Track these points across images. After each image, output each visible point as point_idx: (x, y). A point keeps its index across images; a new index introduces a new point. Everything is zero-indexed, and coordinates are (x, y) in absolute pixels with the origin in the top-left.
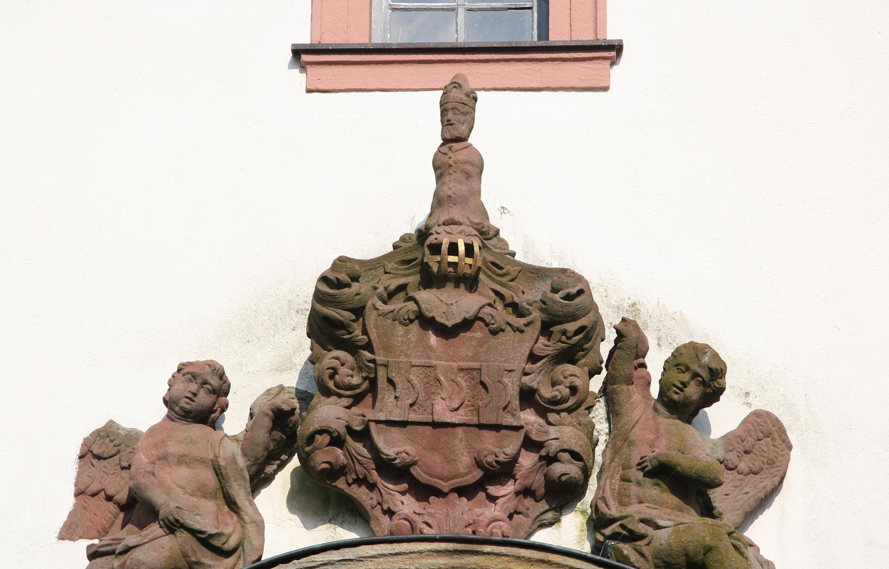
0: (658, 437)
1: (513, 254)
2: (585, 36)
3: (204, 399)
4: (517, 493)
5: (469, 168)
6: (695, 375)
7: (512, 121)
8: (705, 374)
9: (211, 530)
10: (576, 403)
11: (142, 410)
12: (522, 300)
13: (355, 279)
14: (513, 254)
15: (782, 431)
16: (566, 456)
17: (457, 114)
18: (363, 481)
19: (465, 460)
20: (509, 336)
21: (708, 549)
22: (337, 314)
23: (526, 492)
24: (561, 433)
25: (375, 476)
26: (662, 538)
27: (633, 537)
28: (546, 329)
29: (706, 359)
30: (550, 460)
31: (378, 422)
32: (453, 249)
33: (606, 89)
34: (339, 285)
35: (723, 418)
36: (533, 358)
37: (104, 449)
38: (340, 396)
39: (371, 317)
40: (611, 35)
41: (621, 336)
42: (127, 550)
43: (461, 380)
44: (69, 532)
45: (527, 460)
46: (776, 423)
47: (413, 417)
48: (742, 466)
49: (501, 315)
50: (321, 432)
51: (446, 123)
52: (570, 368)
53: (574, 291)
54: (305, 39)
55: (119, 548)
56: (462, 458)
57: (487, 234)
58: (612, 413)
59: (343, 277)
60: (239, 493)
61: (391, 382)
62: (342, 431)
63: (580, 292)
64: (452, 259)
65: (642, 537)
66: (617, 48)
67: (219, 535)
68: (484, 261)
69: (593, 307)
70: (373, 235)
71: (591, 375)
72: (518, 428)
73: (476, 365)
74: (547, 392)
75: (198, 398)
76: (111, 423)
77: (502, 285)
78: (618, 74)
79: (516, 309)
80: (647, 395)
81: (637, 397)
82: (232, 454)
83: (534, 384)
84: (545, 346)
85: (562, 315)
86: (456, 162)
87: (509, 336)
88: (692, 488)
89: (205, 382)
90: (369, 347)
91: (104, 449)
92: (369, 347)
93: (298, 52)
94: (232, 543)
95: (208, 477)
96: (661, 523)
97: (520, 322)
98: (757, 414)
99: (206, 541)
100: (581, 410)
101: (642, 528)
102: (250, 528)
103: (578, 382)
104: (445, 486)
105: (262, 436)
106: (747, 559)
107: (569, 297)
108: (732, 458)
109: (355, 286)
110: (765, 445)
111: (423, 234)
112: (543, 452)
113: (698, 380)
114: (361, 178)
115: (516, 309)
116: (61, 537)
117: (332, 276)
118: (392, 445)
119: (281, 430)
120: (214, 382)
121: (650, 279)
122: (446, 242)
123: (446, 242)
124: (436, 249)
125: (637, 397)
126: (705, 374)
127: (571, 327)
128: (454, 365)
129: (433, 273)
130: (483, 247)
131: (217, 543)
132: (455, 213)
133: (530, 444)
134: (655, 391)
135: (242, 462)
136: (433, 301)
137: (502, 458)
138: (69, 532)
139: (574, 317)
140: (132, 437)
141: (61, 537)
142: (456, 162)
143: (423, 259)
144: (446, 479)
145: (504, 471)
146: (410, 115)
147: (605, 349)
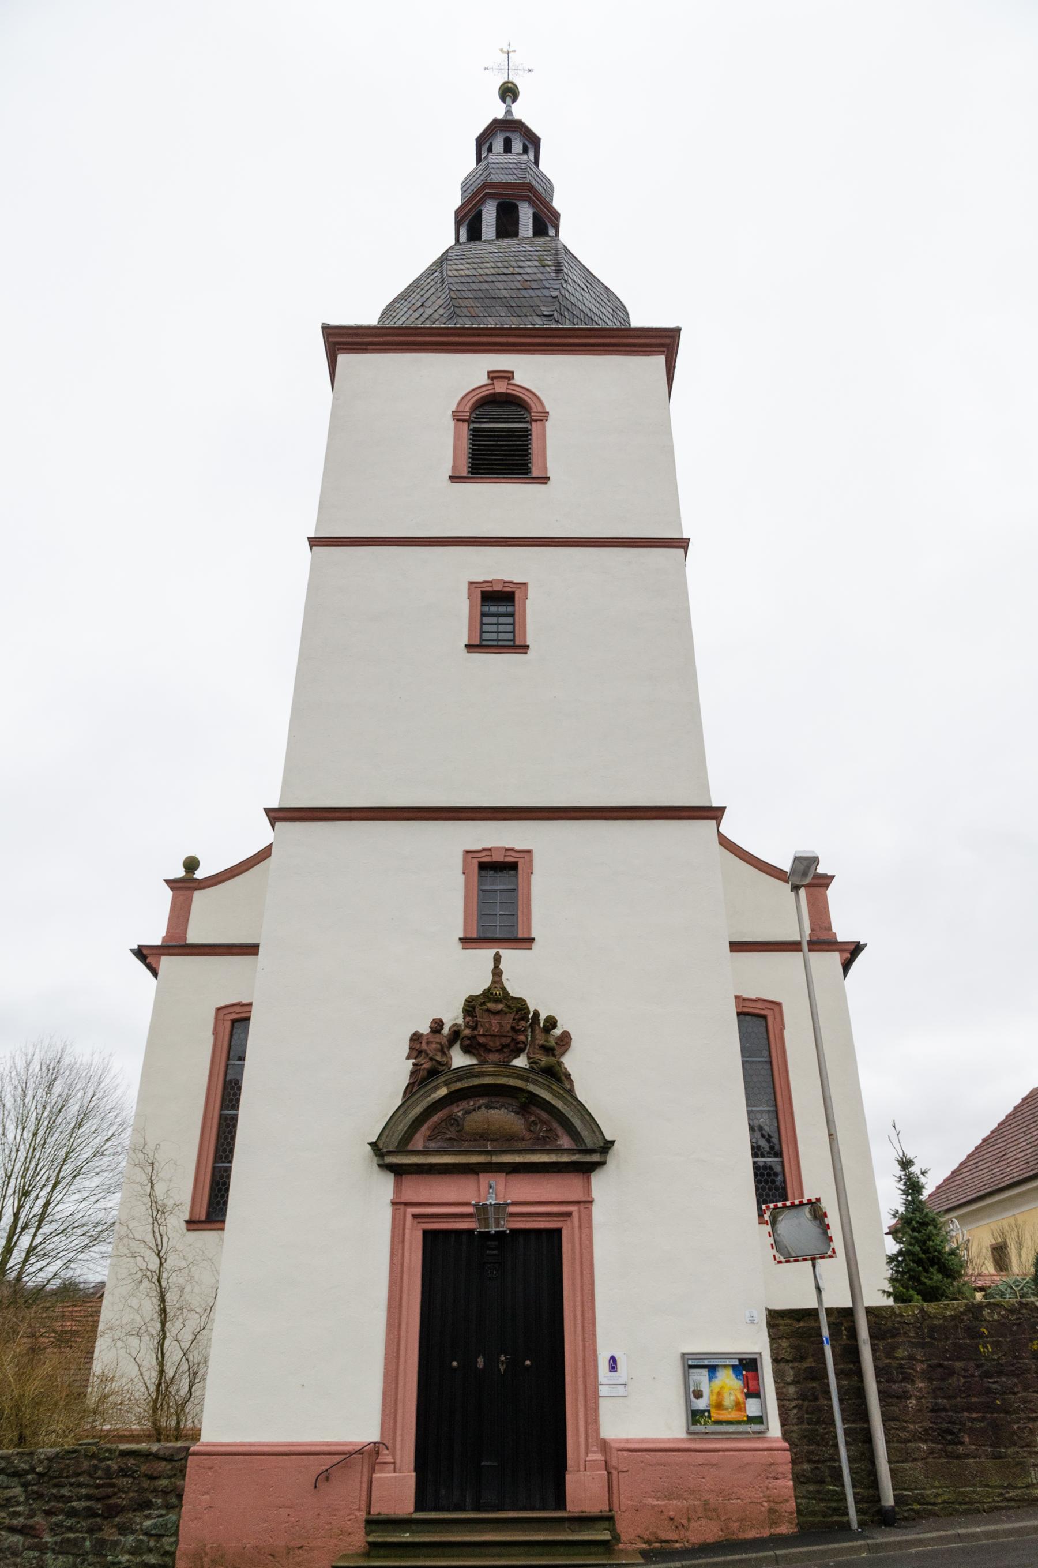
0: (540, 1039)
2: (526, 936)
7: (510, 957)
11: (425, 1029)
19: (498, 1044)
22: (471, 1006)
23: (512, 1051)
24: (522, 1038)
28: (517, 1013)
35: (557, 1032)
37: (416, 1038)
39: (477, 1010)
44: (408, 1058)
49: (506, 1010)
57: (504, 989)
60: (446, 1050)
75: (437, 1026)
78: (534, 945)
82: (445, 1041)
85: (519, 1007)
86: (497, 973)
88: (548, 1050)
95: (439, 1046)
99: (439, 1063)
110: (565, 1040)
113: (552, 1023)
114: (473, 971)
116: (265, 809)
118: (481, 1040)
119: (456, 1035)
121: (541, 1002)
129: (484, 1357)
136: (491, 1005)
138: (408, 1058)
140: (422, 1035)
141: (265, 809)
142: (497, 973)
143: (487, 994)
145: (508, 1046)
146: (485, 956)
147: (530, 1016)
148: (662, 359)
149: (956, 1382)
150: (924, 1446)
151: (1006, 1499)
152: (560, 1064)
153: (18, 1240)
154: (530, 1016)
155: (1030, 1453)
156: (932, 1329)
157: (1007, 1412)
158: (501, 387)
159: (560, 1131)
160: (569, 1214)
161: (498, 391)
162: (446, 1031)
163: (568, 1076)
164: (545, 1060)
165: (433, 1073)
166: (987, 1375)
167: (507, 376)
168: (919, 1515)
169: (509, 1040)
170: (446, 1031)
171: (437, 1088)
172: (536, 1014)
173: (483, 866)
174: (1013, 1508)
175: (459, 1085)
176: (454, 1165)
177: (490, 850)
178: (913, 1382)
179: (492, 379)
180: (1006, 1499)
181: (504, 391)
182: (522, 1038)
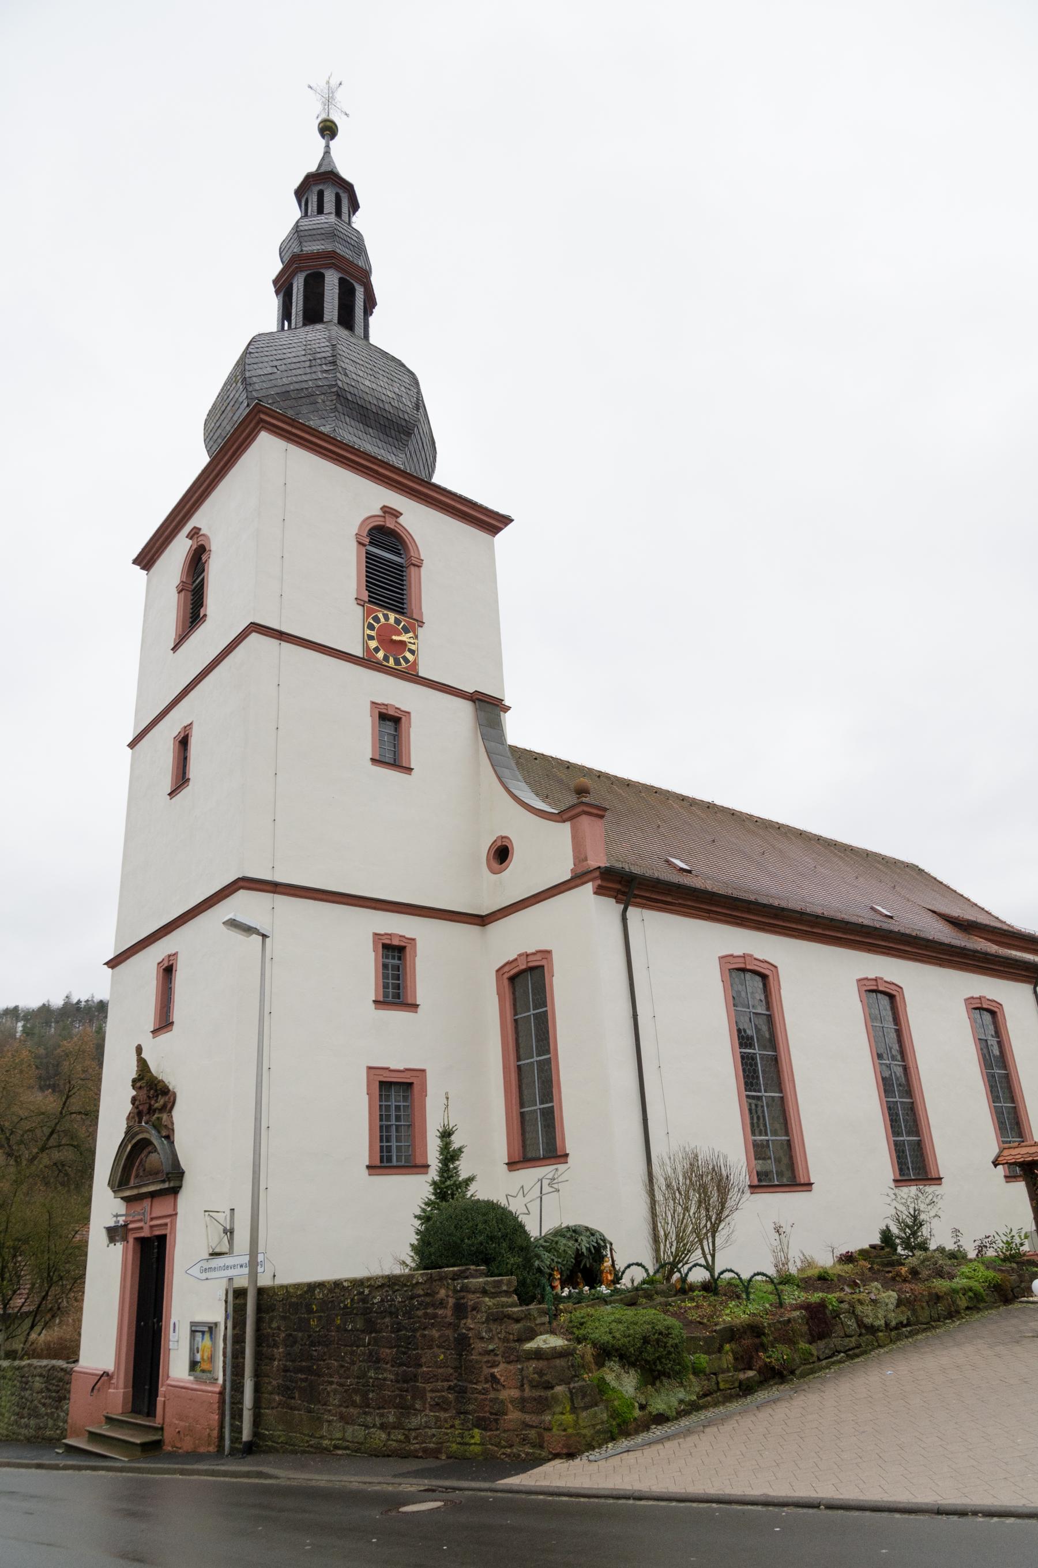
148: (622, 906)
149: (297, 1348)
150: (277, 1398)
151: (312, 1446)
153: (835, 854)
155: (325, 1410)
156: (292, 1304)
157: (319, 1376)
158: (390, 524)
160: (166, 1224)
161: (388, 525)
166: (313, 1344)
167: (396, 514)
168: (270, 1450)
173: (386, 947)
174: (312, 1453)
175: (134, 1141)
176: (161, 1190)
177: (390, 935)
178: (278, 1348)
179: (385, 512)
180: (312, 1446)
181: (392, 527)
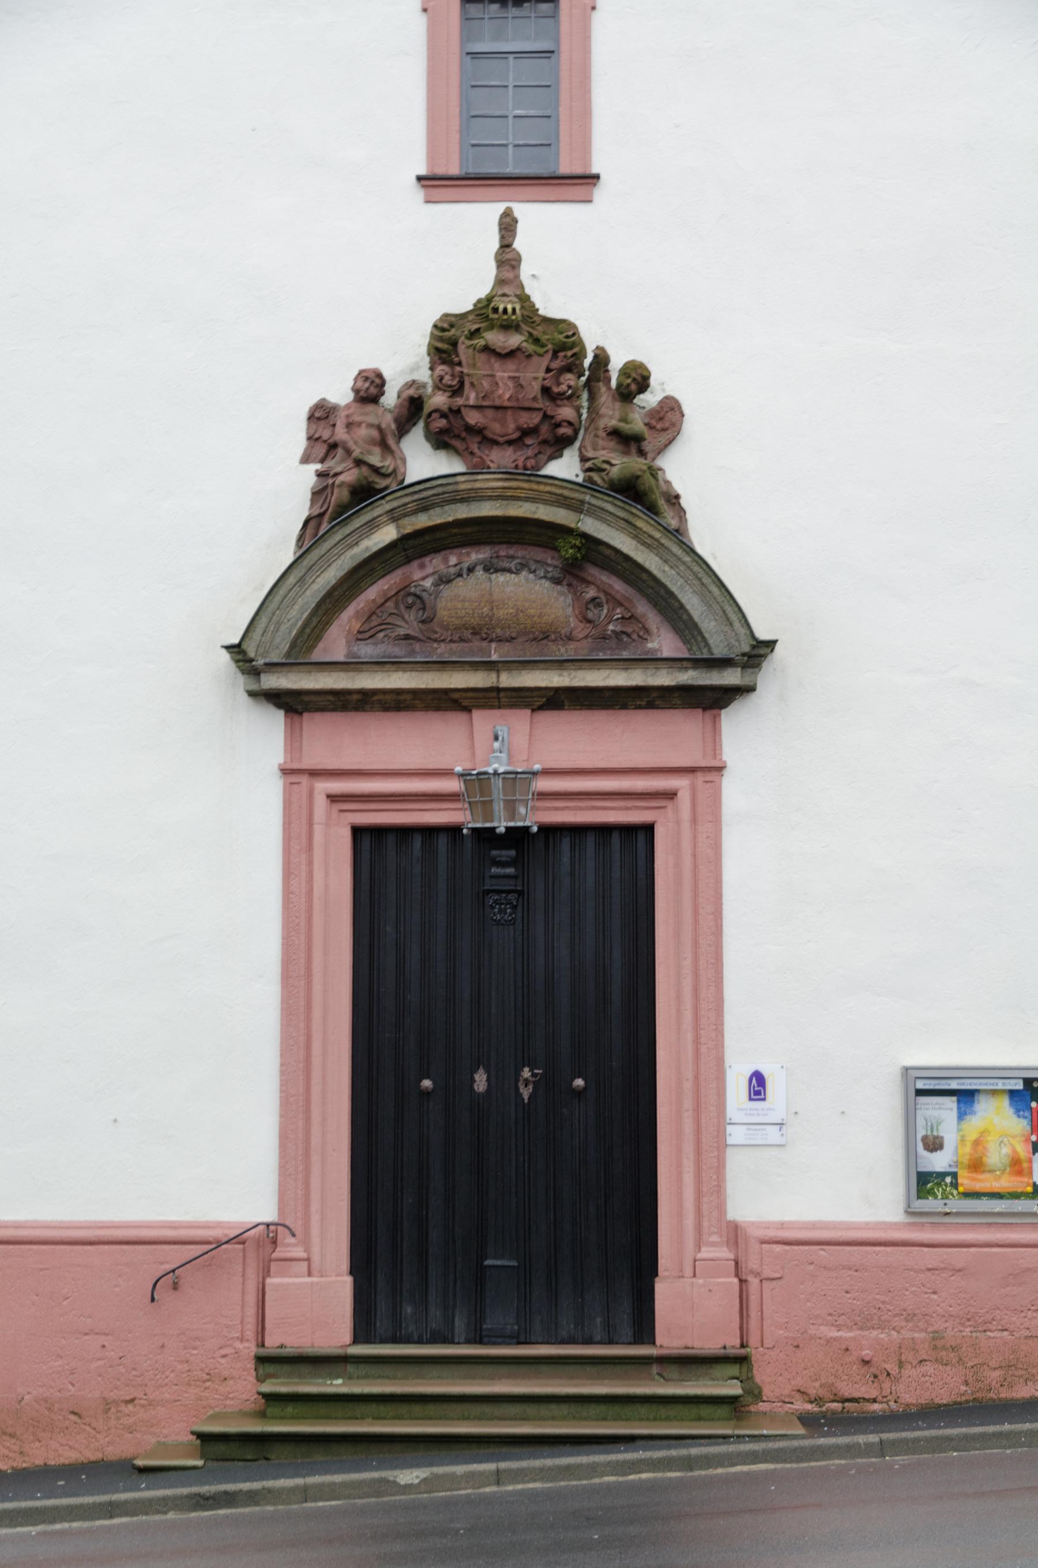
1: (538, 310)
2: (578, 170)
3: (373, 391)
4: (540, 443)
5: (513, 263)
6: (634, 380)
7: (540, 222)
8: (639, 378)
9: (379, 465)
10: (572, 397)
11: (341, 394)
12: (544, 338)
13: (452, 326)
14: (538, 310)
15: (680, 407)
16: (565, 424)
17: (508, 226)
18: (458, 437)
19: (512, 426)
20: (535, 358)
21: (638, 477)
22: (447, 342)
23: (545, 442)
25: (464, 434)
26: (615, 472)
27: (601, 470)
28: (555, 354)
29: (639, 371)
30: (558, 425)
31: (466, 406)
32: (505, 310)
33: (590, 201)
34: (443, 330)
35: (649, 399)
36: (548, 370)
37: (321, 414)
38: (445, 391)
39: (461, 348)
40: (594, 171)
41: (596, 356)
42: (336, 475)
43: (511, 384)
44: (306, 459)
45: (545, 429)
46: (676, 401)
47: (485, 403)
48: (659, 426)
49: (530, 348)
50: (435, 411)
51: (502, 237)
52: (569, 376)
53: (570, 333)
54: (423, 171)
55: (332, 473)
56: (510, 426)
57: (525, 299)
58: (592, 398)
59: (446, 326)
60: (391, 442)
61: (472, 384)
62: (446, 410)
63: (574, 334)
64: (505, 317)
65: (604, 470)
66: (597, 177)
67: (382, 467)
68: (523, 315)
69: (581, 340)
70: (462, 300)
71: (579, 377)
72: (539, 409)
73: (517, 374)
74: (556, 390)
75: (370, 388)
76: (324, 400)
77: (533, 328)
79: (537, 341)
80: (609, 388)
81: (603, 389)
82: (388, 421)
83: (548, 385)
84: (556, 365)
85: (561, 343)
86: (508, 259)
87: (535, 358)
89: (373, 382)
90: (460, 364)
91: (321, 414)
92: (460, 364)
93: (419, 179)
94: (390, 470)
95: (375, 433)
96: (614, 462)
97: (541, 351)
98: (667, 398)
99: (376, 470)
100: (574, 398)
101: (605, 466)
102: (399, 462)
103: (572, 383)
104: (501, 440)
105: (405, 412)
106: (657, 480)
107: (567, 337)
108: (653, 422)
109: (453, 331)
110: (668, 418)
111: (489, 299)
112: (553, 421)
113: (637, 379)
115: (537, 341)
117: (440, 325)
118: (473, 418)
119: (413, 407)
120: (378, 381)
121: (611, 332)
122: (501, 308)
123: (501, 308)
124: (495, 310)
125: (603, 389)
126: (639, 378)
127: (569, 353)
128: (506, 375)
130: (522, 308)
131: (383, 471)
132: (506, 290)
133: (546, 417)
134: (614, 383)
135: (393, 426)
136: (494, 338)
137: (531, 425)
138: (306, 459)
139: (571, 348)
142: (508, 259)
144: (502, 436)
145: (533, 431)
147: (587, 362)
152: (654, 472)
154: (587, 362)
159: (652, 619)
162: (390, 398)
163: (674, 499)
164: (621, 464)
165: (363, 494)
169: (535, 419)
170: (390, 398)
171: (372, 526)
172: (601, 360)
182: (566, 412)
